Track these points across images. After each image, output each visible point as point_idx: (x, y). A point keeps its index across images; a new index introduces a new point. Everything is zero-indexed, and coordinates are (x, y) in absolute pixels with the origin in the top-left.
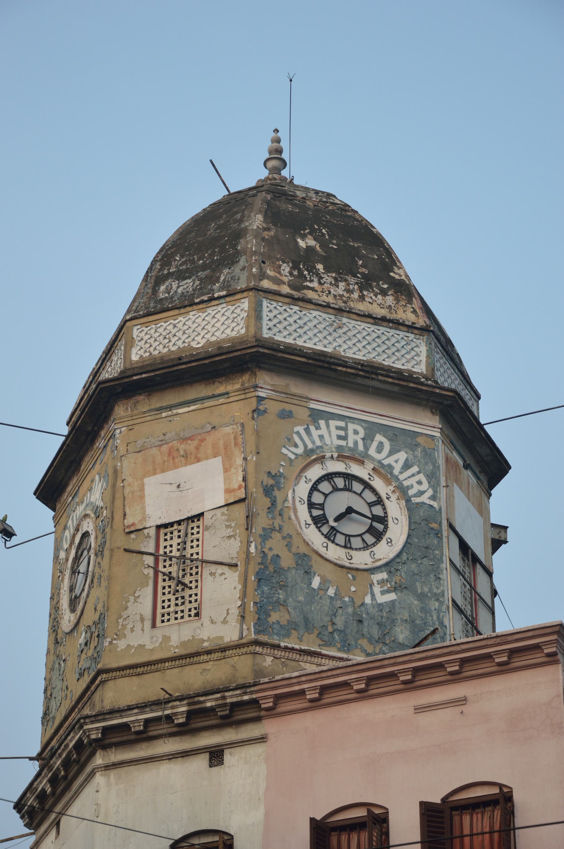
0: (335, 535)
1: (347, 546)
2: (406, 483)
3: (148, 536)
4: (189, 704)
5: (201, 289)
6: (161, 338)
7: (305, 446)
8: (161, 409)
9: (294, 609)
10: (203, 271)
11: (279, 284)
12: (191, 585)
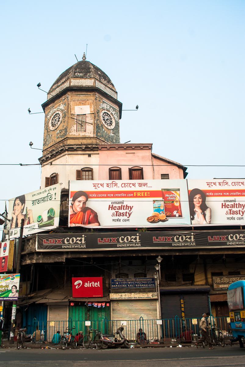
1: (107, 125)
2: (115, 117)
3: (75, 116)
8: (78, 95)
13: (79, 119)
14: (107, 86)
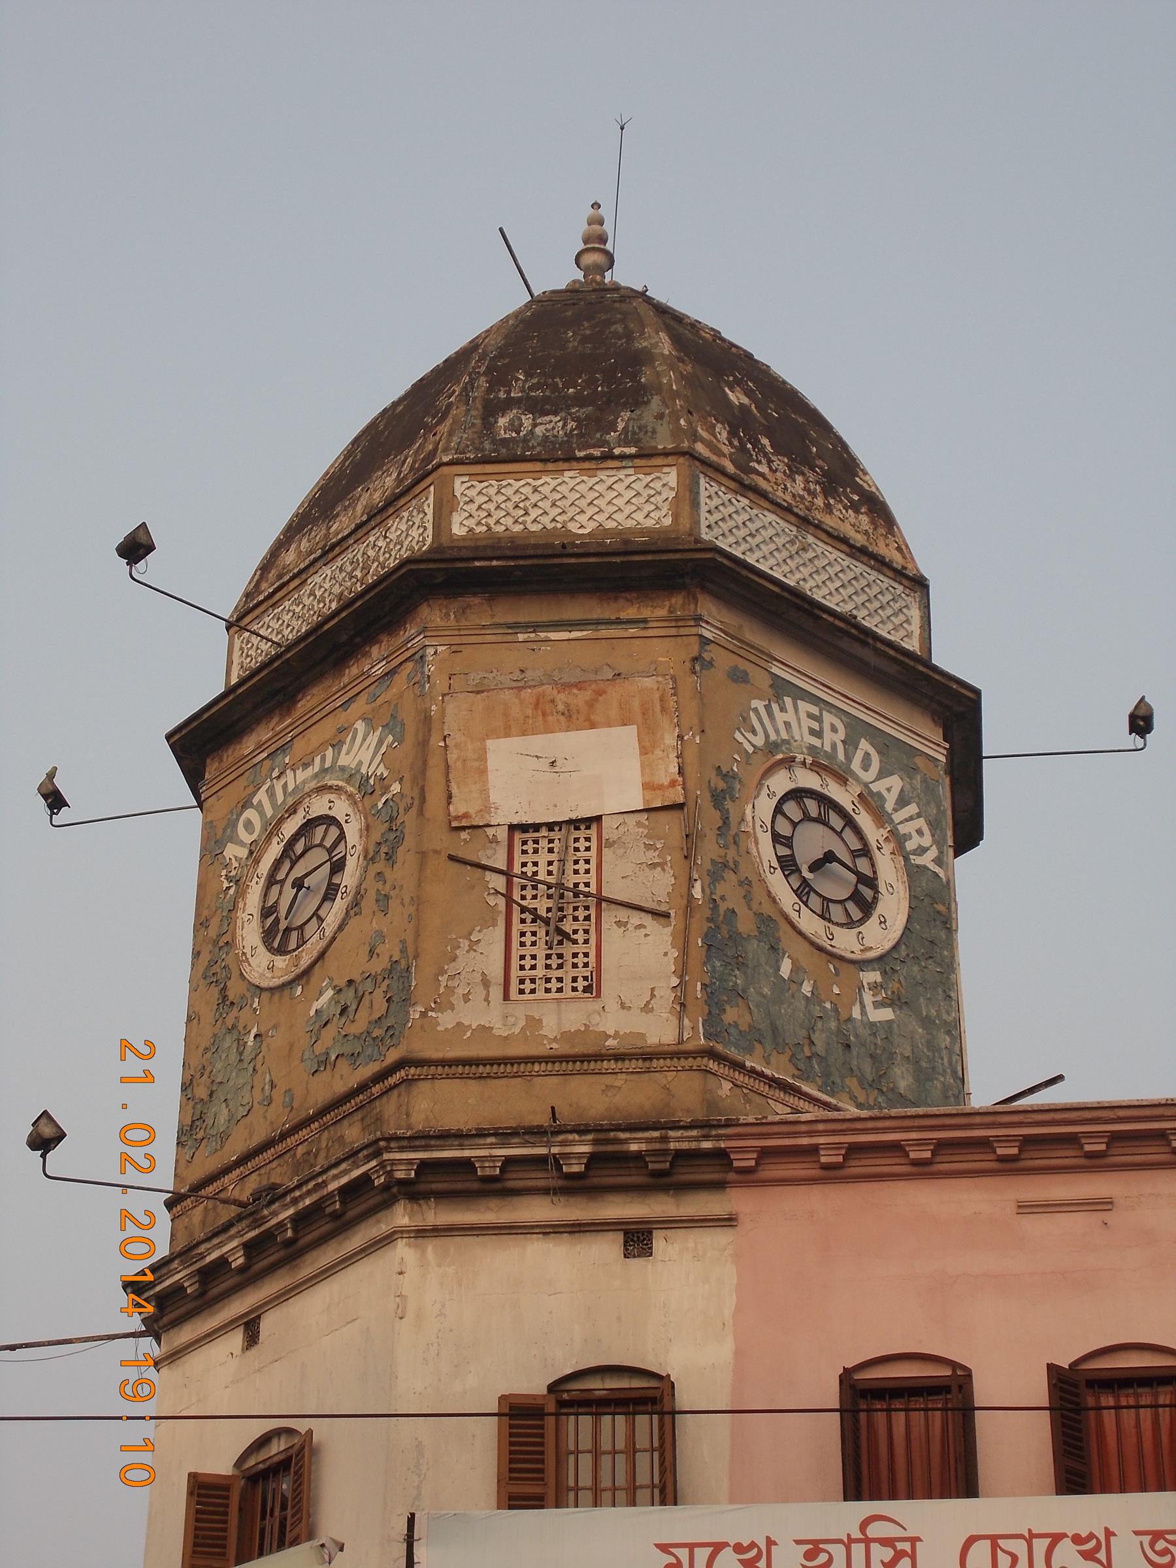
0: (808, 893)
2: (903, 829)
3: (494, 840)
4: (595, 1142)
5: (581, 435)
6: (510, 505)
7: (767, 736)
8: (517, 627)
9: (757, 1006)
10: (581, 406)
11: (719, 456)
12: (575, 937)
13: (529, 870)
14: (818, 527)
